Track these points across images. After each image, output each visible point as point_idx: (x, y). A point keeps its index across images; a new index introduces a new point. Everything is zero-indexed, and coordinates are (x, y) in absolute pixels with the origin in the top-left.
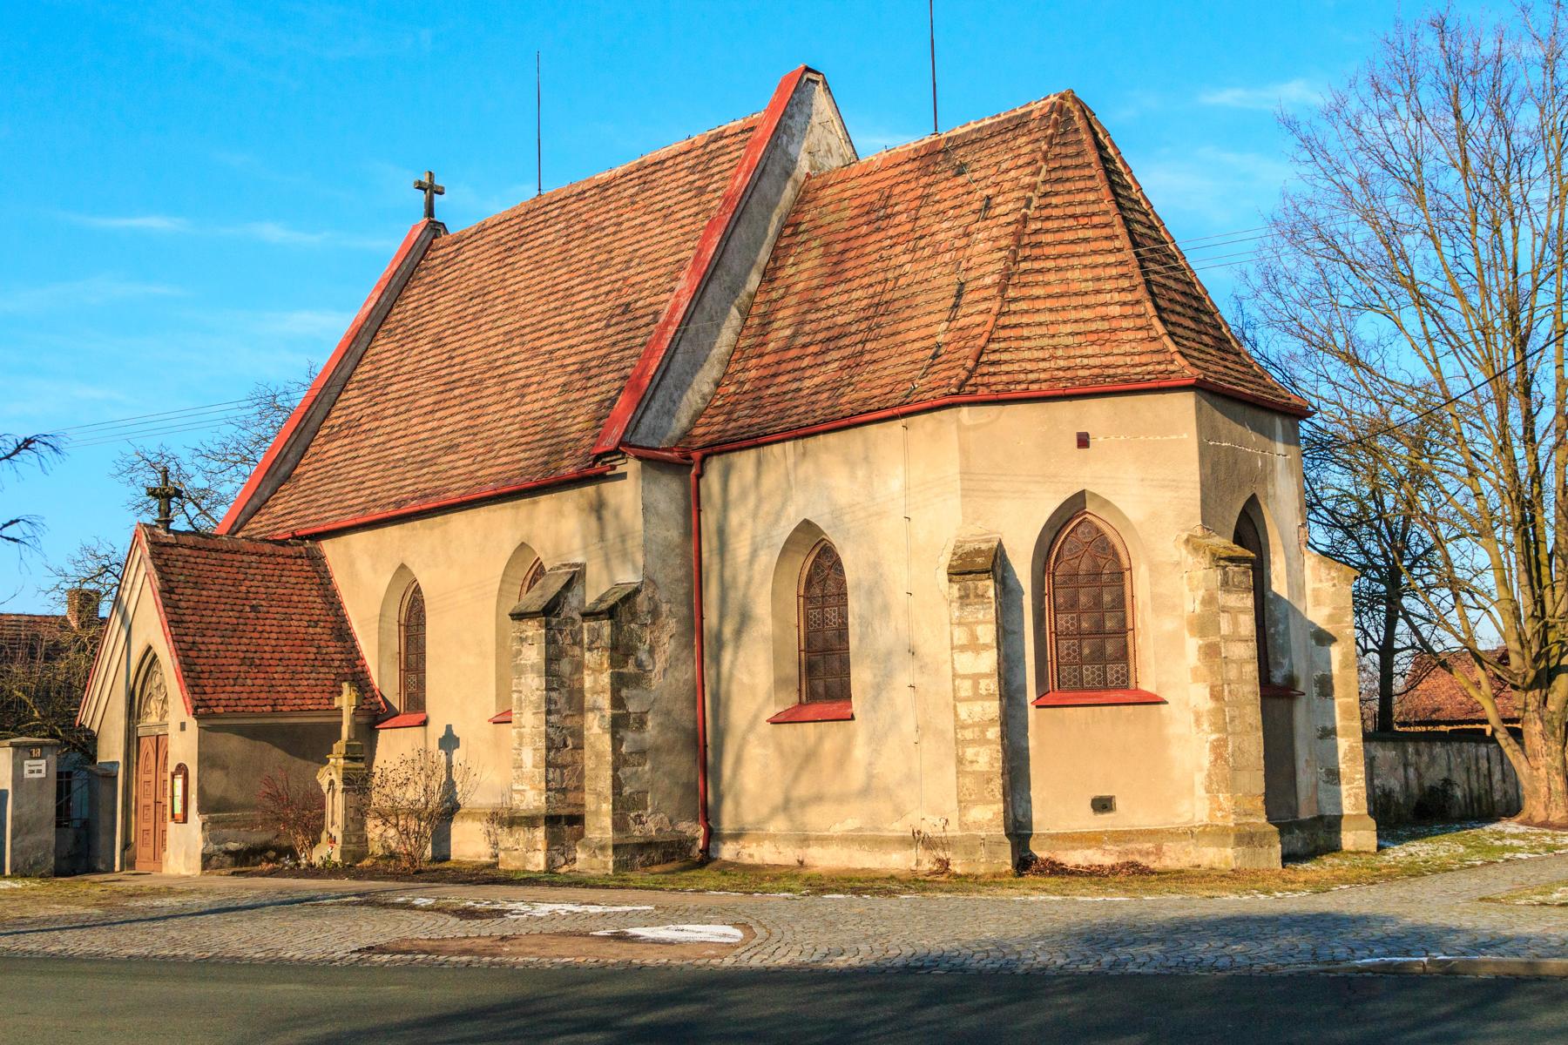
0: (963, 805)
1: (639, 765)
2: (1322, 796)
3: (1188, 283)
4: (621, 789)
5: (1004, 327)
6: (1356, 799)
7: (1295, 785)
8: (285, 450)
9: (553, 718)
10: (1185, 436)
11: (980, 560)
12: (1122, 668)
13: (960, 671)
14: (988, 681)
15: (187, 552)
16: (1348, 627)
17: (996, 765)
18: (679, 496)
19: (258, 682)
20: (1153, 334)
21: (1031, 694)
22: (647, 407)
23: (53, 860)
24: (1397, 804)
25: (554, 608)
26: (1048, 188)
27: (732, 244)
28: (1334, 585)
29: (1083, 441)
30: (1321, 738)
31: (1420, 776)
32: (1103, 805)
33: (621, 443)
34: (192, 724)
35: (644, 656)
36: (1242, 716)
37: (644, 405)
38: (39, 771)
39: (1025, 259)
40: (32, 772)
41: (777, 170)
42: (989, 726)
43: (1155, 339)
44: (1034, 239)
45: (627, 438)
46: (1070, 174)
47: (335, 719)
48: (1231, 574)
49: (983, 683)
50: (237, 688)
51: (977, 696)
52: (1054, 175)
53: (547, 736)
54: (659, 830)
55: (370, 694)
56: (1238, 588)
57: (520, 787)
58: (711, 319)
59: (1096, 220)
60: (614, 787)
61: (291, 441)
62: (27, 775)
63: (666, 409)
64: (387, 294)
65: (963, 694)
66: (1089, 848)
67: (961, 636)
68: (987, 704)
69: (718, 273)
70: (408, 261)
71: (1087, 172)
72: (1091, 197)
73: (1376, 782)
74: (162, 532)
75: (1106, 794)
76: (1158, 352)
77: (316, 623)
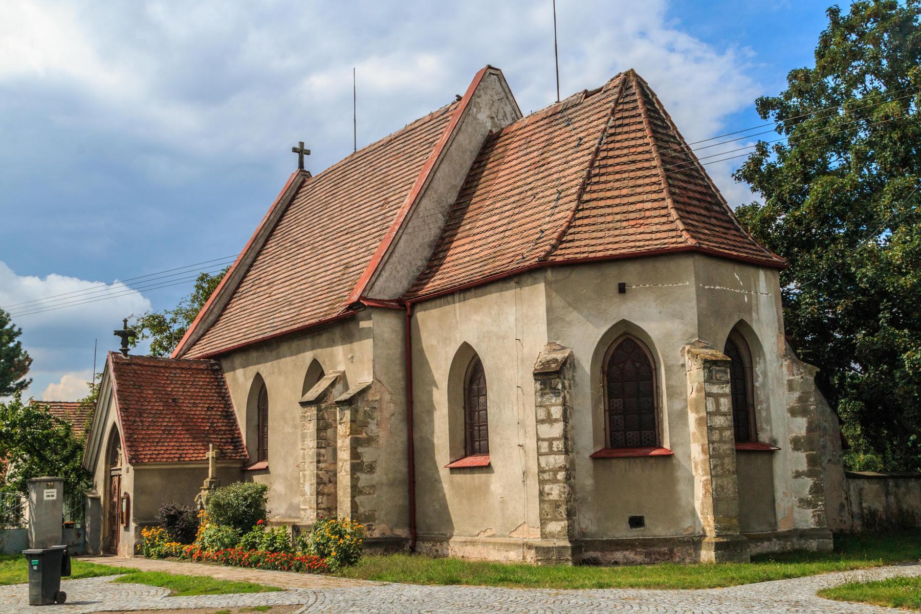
0: (543, 522)
2: (796, 515)
3: (705, 187)
4: (357, 509)
5: (579, 219)
6: (819, 518)
7: (774, 509)
8: (212, 307)
9: (322, 465)
10: (687, 283)
11: (553, 366)
12: (652, 434)
13: (542, 436)
14: (558, 442)
15: (136, 367)
16: (812, 405)
17: (563, 496)
18: (398, 329)
19: (172, 444)
20: (671, 219)
21: (442, 456)
22: (379, 275)
24: (881, 519)
25: (323, 398)
26: (613, 131)
27: (438, 174)
28: (802, 377)
29: (622, 289)
30: (795, 477)
31: (898, 501)
32: (636, 522)
33: (361, 297)
34: (131, 468)
36: (722, 464)
37: (377, 274)
38: (53, 496)
39: (595, 175)
40: (48, 496)
42: (559, 471)
43: (672, 222)
44: (603, 162)
45: (365, 295)
46: (627, 121)
47: (203, 466)
49: (555, 443)
50: (159, 448)
51: (551, 452)
52: (618, 123)
53: (318, 476)
55: (240, 450)
56: (719, 382)
57: (304, 507)
58: (424, 221)
60: (352, 508)
61: (216, 301)
62: (45, 498)
64: (274, 214)
65: (543, 450)
66: (627, 550)
67: (542, 414)
68: (557, 457)
69: (429, 192)
70: (287, 195)
71: (638, 119)
72: (639, 134)
73: (864, 505)
74: (122, 355)
76: (673, 230)
77: (212, 408)
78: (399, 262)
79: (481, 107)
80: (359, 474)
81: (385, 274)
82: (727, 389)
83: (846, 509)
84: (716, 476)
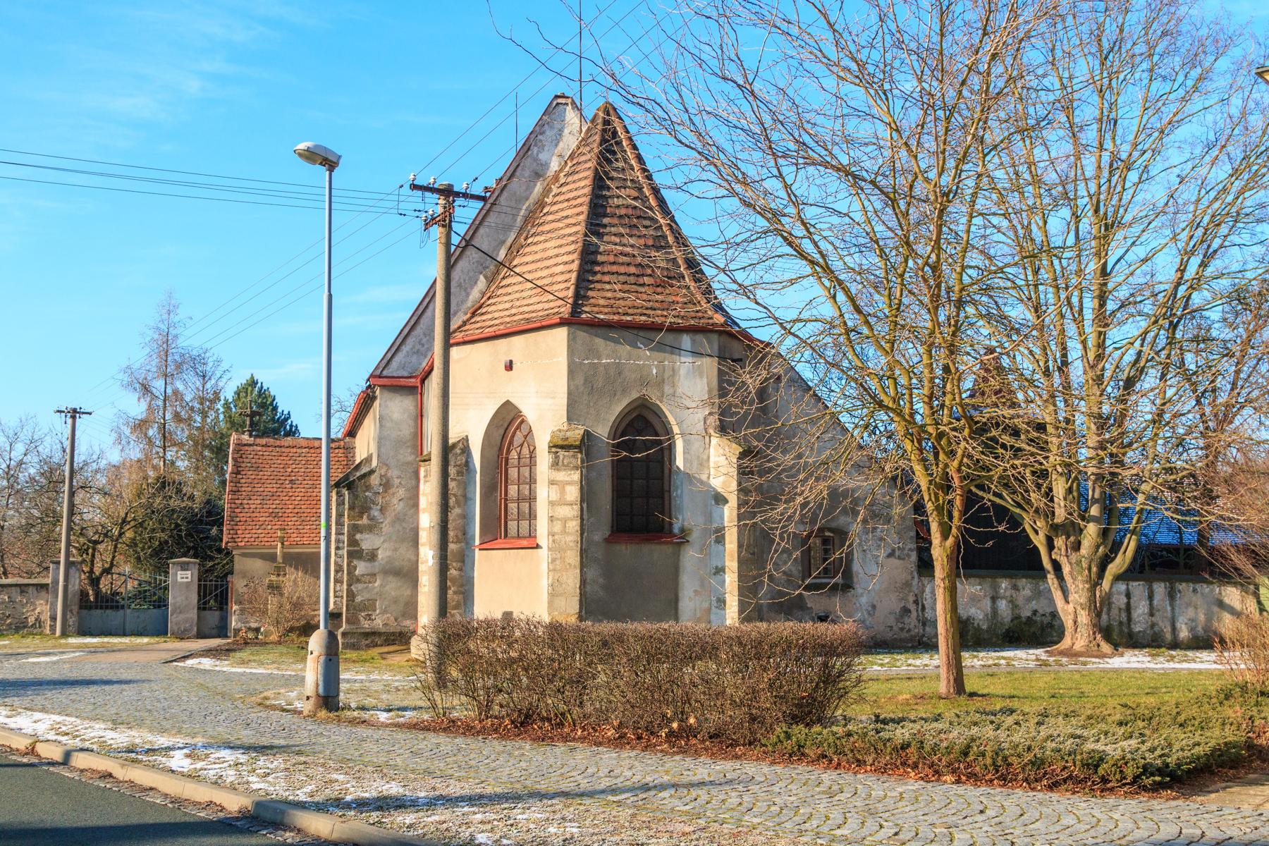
1: (370, 582)
23: (195, 629)
24: (979, 629)
29: (509, 366)
35: (375, 513)
41: (527, 173)
48: (561, 457)
54: (385, 625)
56: (566, 467)
59: (574, 202)
62: (179, 580)
63: (415, 350)
75: (509, 610)
78: (425, 334)
79: (544, 146)
80: (355, 562)
81: (405, 349)
82: (576, 476)
83: (914, 614)
84: (554, 570)
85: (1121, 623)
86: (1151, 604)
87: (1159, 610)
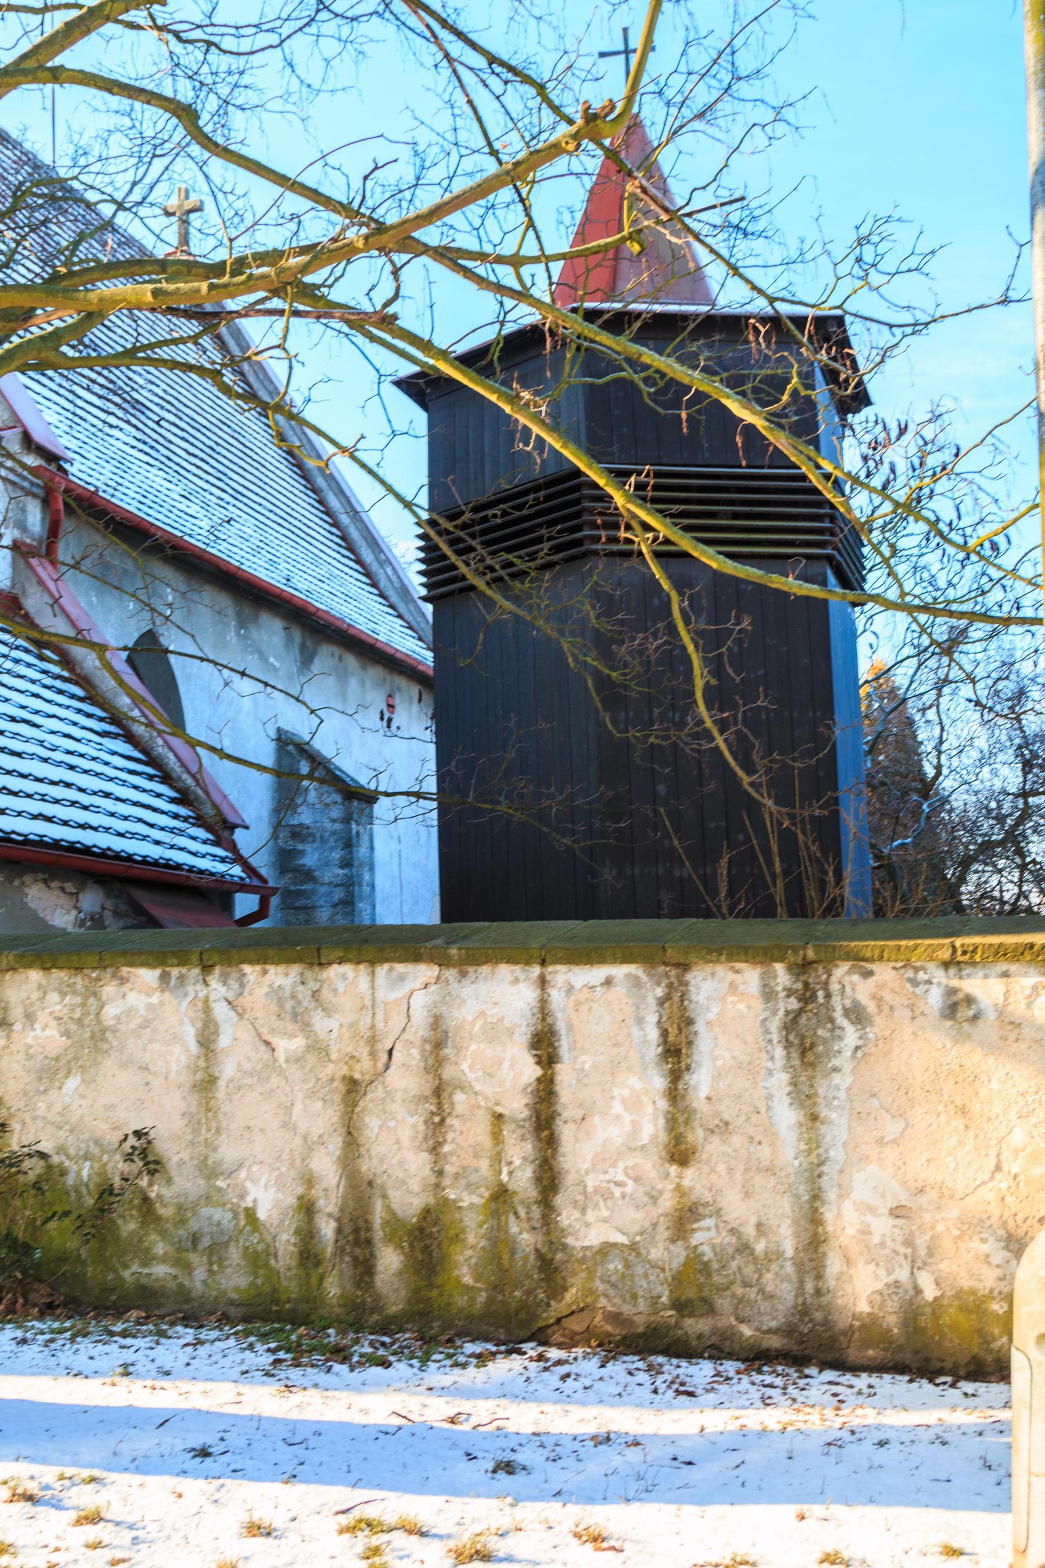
85: (501, 1196)
86: (675, 1094)
87: (724, 1127)
